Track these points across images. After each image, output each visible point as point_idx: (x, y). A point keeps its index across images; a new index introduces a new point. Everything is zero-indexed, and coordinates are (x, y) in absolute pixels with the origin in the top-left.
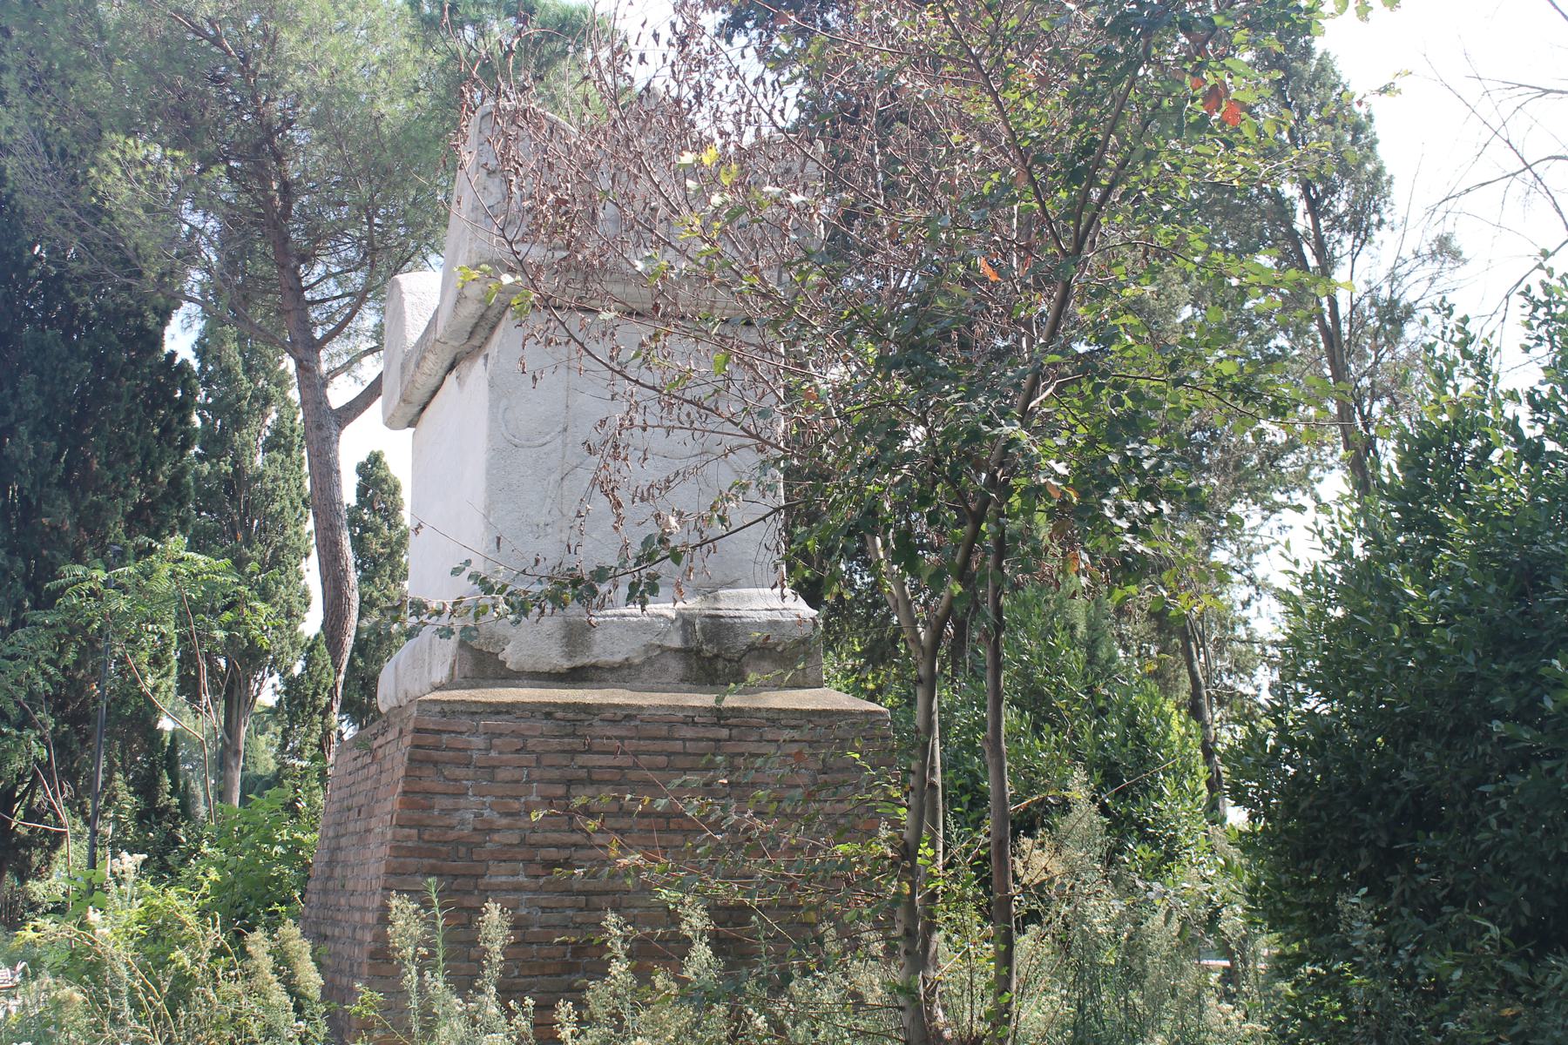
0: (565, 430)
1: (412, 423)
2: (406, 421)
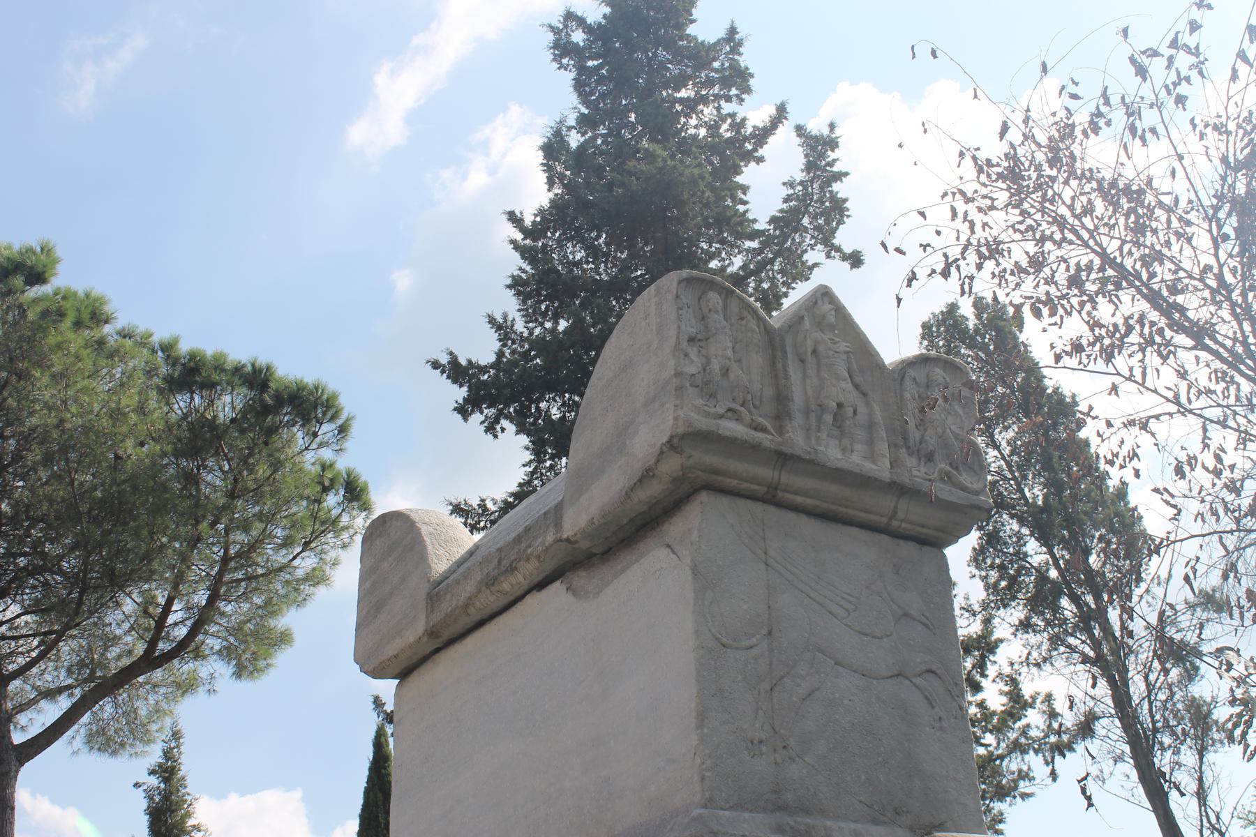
0: (770, 633)
1: (403, 675)
2: (397, 670)
